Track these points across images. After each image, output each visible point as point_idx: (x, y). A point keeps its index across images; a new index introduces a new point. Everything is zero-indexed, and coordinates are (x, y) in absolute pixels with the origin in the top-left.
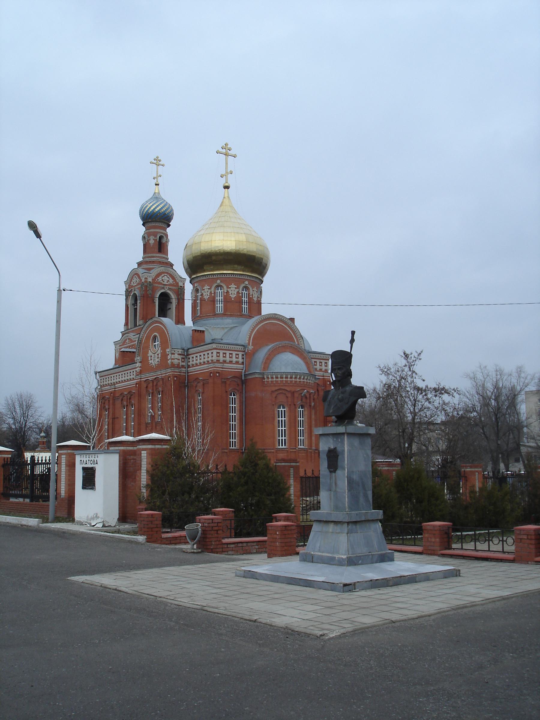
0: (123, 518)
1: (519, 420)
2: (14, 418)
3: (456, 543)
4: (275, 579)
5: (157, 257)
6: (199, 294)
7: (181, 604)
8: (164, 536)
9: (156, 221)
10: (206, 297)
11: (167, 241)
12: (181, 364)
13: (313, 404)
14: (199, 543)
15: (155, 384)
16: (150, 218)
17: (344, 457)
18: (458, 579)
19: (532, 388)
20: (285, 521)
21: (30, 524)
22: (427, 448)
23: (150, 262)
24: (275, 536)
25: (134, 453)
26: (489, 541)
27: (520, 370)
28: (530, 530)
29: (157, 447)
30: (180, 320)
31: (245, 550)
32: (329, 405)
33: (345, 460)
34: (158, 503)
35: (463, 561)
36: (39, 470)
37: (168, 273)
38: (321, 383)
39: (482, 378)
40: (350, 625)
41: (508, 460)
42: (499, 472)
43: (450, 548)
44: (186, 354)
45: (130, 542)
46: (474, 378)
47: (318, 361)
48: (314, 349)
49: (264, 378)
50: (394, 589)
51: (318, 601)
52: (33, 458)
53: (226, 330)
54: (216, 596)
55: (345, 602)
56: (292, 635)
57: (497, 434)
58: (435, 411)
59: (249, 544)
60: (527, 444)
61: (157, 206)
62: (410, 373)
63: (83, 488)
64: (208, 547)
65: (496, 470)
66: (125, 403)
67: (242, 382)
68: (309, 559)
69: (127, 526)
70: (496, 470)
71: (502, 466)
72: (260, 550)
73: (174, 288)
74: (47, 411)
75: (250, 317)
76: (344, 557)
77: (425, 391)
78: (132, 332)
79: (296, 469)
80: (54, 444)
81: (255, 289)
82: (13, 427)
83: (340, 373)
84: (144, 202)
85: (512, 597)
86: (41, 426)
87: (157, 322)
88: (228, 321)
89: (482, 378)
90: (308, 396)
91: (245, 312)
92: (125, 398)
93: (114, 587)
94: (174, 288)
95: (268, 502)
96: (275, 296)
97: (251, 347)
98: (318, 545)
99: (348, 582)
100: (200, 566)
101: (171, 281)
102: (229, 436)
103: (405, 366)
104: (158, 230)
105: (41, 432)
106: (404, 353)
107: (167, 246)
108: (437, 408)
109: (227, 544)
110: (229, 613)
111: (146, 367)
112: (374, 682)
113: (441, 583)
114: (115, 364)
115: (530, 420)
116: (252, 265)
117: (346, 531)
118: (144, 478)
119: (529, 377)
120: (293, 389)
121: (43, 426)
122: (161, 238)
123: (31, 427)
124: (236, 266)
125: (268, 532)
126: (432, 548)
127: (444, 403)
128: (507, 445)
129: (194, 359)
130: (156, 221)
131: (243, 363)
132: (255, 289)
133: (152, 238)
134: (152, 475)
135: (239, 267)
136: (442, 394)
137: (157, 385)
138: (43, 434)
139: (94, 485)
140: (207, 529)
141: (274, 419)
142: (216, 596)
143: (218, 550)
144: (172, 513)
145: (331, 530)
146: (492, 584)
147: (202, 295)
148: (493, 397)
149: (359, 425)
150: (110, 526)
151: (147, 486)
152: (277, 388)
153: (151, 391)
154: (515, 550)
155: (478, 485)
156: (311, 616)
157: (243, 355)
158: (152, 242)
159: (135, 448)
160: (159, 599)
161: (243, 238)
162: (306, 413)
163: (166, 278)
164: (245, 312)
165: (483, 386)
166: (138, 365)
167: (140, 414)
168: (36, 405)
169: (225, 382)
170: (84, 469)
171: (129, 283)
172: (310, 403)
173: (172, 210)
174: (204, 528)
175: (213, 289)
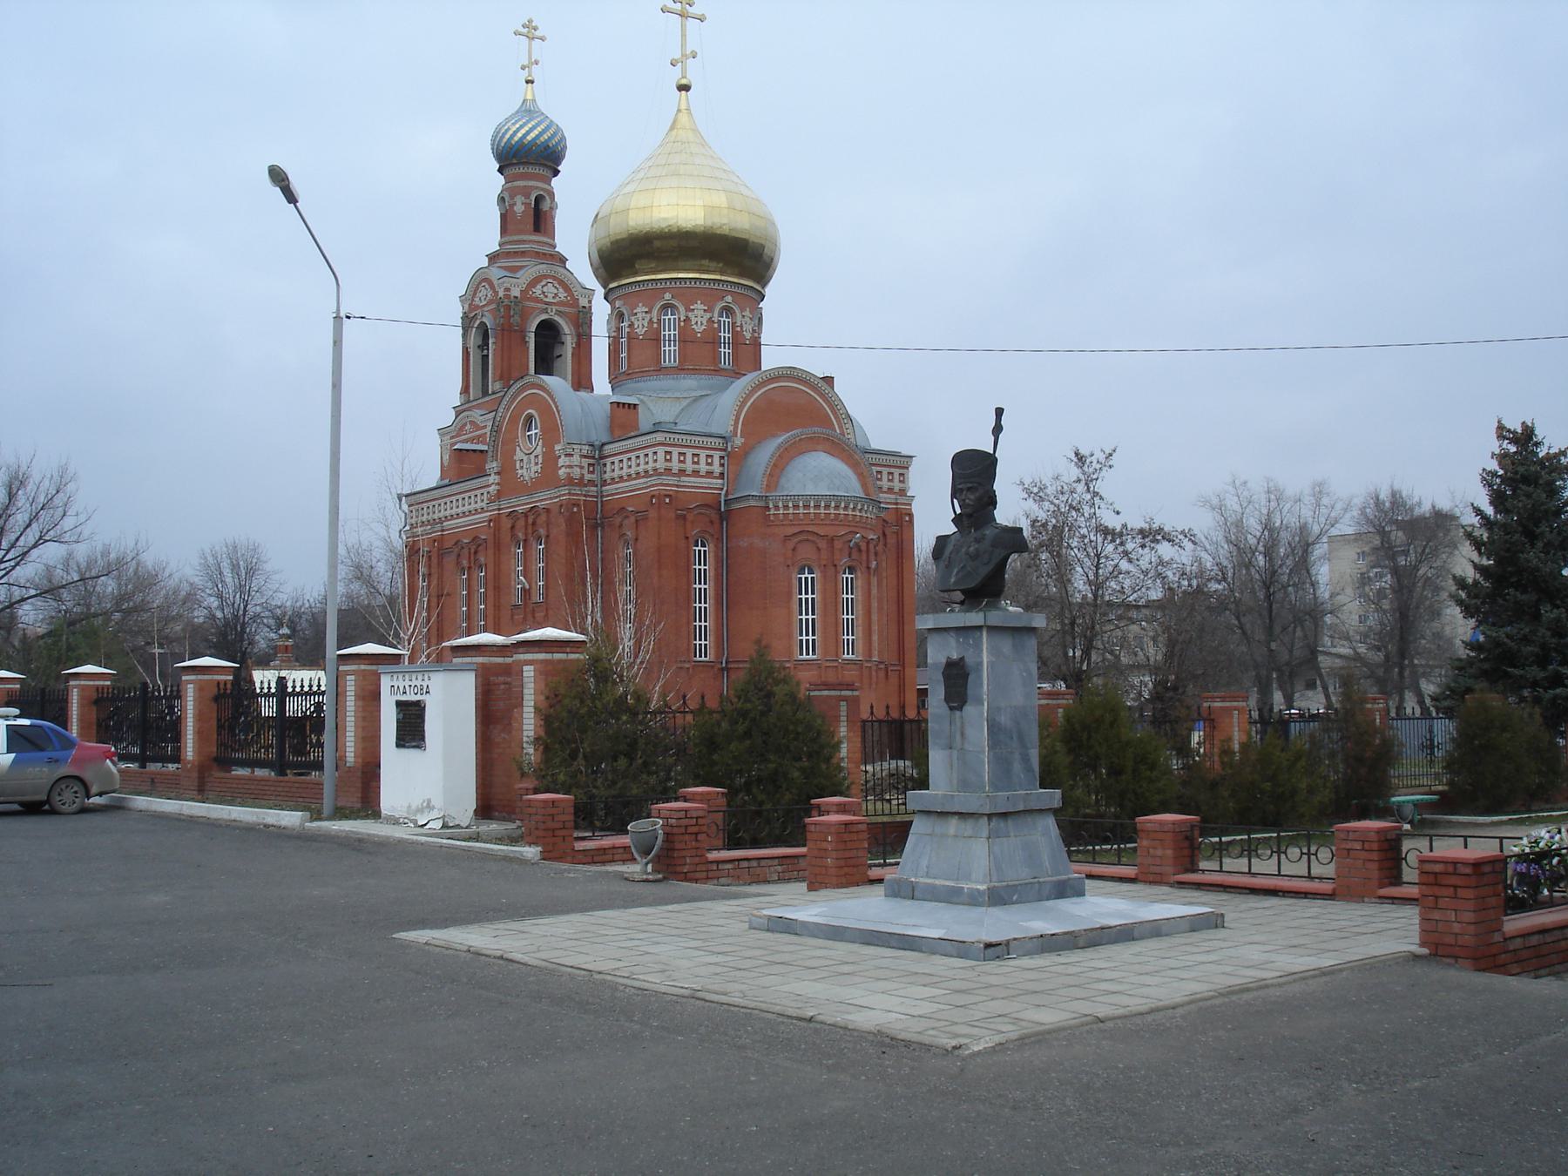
0: (485, 810)
1: (1315, 598)
2: (220, 596)
3: (1209, 858)
4: (836, 933)
5: (532, 241)
6: (626, 324)
7: (646, 986)
8: (579, 846)
9: (529, 161)
10: (640, 331)
11: (553, 208)
12: (588, 477)
13: (874, 564)
14: (657, 860)
15: (530, 521)
16: (514, 156)
17: (980, 677)
18: (1221, 933)
19: (1346, 528)
20: (837, 812)
21: (284, 823)
22: (1117, 657)
23: (516, 254)
24: (824, 845)
25: (507, 670)
26: (1279, 853)
27: (1319, 491)
28: (1369, 830)
29: (557, 656)
30: (582, 381)
31: (755, 875)
32: (949, 566)
33: (983, 684)
34: (562, 777)
35: (1224, 896)
36: (294, 707)
37: (554, 278)
38: (891, 518)
39: (1237, 507)
40: (1011, 1027)
41: (1292, 684)
42: (1271, 709)
43: (1194, 870)
44: (597, 456)
45: (507, 859)
46: (1220, 508)
47: (885, 471)
48: (875, 444)
49: (768, 508)
50: (1089, 953)
51: (935, 979)
52: (281, 682)
53: (685, 403)
54: (719, 969)
55: (993, 980)
56: (892, 1047)
57: (1269, 630)
58: (1136, 577)
59: (763, 863)
60: (1333, 650)
61: (531, 130)
62: (1088, 497)
63: (398, 746)
64: (679, 869)
65: (1265, 705)
66: (465, 563)
67: (721, 517)
68: (906, 891)
69: (494, 827)
70: (1265, 705)
71: (1278, 697)
72: (787, 875)
73: (567, 310)
74: (299, 577)
75: (738, 374)
76: (982, 887)
77: (1121, 535)
78: (478, 407)
79: (853, 703)
80: (332, 651)
81: (747, 313)
82: (219, 614)
83: (971, 498)
84: (501, 119)
85: (1341, 970)
86: (279, 612)
87: (534, 386)
88: (689, 383)
89: (1237, 507)
90: (864, 547)
91: (725, 364)
92: (466, 551)
93: (499, 953)
94: (567, 310)
95: (796, 774)
96: (794, 327)
97: (739, 441)
98: (924, 863)
99: (993, 939)
100: (670, 907)
101: (562, 295)
102: (693, 633)
103: (1079, 481)
104: (531, 183)
105: (280, 625)
106: (1077, 454)
107: (553, 218)
108: (1145, 573)
109: (718, 862)
110: (753, 1005)
111: (510, 484)
112: (1080, 1140)
113: (1183, 941)
114: (442, 478)
115: (1341, 599)
116: (740, 259)
117: (985, 833)
118: (529, 724)
119: (1339, 506)
120: (830, 531)
121: (284, 614)
122: (539, 199)
123: (257, 616)
124: (706, 262)
125: (809, 836)
126: (1157, 869)
127: (1161, 562)
128: (1291, 651)
129: (616, 466)
130: (529, 161)
131: (722, 474)
132: (747, 313)
133: (519, 199)
134: (547, 719)
135: (713, 265)
136: (1158, 541)
137: (534, 524)
138: (285, 631)
139: (423, 739)
140: (675, 830)
141: (789, 595)
142: (719, 969)
143: (698, 875)
144: (592, 797)
145: (952, 831)
146: (1295, 942)
147: (631, 326)
148: (1261, 548)
149: (1011, 610)
150: (458, 826)
151: (537, 739)
152: (797, 530)
153: (521, 535)
154: (1337, 872)
155: (1237, 738)
156: (926, 1008)
157: (722, 458)
158: (519, 208)
159: (508, 660)
160: (597, 977)
161: (720, 200)
162: (859, 583)
163: (550, 289)
164: (725, 364)
165: (1239, 524)
166: (493, 479)
167: (498, 586)
168: (268, 567)
169: (684, 517)
170: (399, 704)
171: (469, 299)
172: (868, 561)
173: (563, 138)
174: (668, 829)
175: (655, 312)
